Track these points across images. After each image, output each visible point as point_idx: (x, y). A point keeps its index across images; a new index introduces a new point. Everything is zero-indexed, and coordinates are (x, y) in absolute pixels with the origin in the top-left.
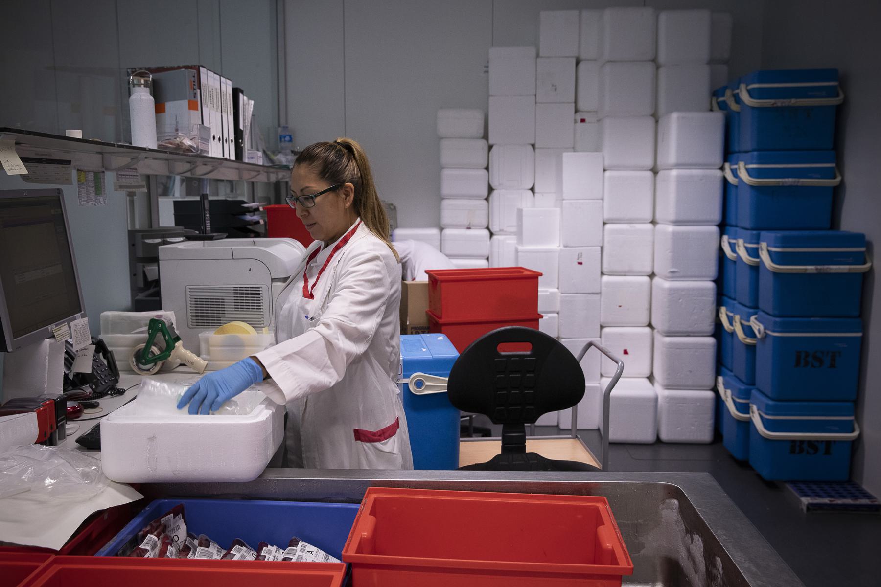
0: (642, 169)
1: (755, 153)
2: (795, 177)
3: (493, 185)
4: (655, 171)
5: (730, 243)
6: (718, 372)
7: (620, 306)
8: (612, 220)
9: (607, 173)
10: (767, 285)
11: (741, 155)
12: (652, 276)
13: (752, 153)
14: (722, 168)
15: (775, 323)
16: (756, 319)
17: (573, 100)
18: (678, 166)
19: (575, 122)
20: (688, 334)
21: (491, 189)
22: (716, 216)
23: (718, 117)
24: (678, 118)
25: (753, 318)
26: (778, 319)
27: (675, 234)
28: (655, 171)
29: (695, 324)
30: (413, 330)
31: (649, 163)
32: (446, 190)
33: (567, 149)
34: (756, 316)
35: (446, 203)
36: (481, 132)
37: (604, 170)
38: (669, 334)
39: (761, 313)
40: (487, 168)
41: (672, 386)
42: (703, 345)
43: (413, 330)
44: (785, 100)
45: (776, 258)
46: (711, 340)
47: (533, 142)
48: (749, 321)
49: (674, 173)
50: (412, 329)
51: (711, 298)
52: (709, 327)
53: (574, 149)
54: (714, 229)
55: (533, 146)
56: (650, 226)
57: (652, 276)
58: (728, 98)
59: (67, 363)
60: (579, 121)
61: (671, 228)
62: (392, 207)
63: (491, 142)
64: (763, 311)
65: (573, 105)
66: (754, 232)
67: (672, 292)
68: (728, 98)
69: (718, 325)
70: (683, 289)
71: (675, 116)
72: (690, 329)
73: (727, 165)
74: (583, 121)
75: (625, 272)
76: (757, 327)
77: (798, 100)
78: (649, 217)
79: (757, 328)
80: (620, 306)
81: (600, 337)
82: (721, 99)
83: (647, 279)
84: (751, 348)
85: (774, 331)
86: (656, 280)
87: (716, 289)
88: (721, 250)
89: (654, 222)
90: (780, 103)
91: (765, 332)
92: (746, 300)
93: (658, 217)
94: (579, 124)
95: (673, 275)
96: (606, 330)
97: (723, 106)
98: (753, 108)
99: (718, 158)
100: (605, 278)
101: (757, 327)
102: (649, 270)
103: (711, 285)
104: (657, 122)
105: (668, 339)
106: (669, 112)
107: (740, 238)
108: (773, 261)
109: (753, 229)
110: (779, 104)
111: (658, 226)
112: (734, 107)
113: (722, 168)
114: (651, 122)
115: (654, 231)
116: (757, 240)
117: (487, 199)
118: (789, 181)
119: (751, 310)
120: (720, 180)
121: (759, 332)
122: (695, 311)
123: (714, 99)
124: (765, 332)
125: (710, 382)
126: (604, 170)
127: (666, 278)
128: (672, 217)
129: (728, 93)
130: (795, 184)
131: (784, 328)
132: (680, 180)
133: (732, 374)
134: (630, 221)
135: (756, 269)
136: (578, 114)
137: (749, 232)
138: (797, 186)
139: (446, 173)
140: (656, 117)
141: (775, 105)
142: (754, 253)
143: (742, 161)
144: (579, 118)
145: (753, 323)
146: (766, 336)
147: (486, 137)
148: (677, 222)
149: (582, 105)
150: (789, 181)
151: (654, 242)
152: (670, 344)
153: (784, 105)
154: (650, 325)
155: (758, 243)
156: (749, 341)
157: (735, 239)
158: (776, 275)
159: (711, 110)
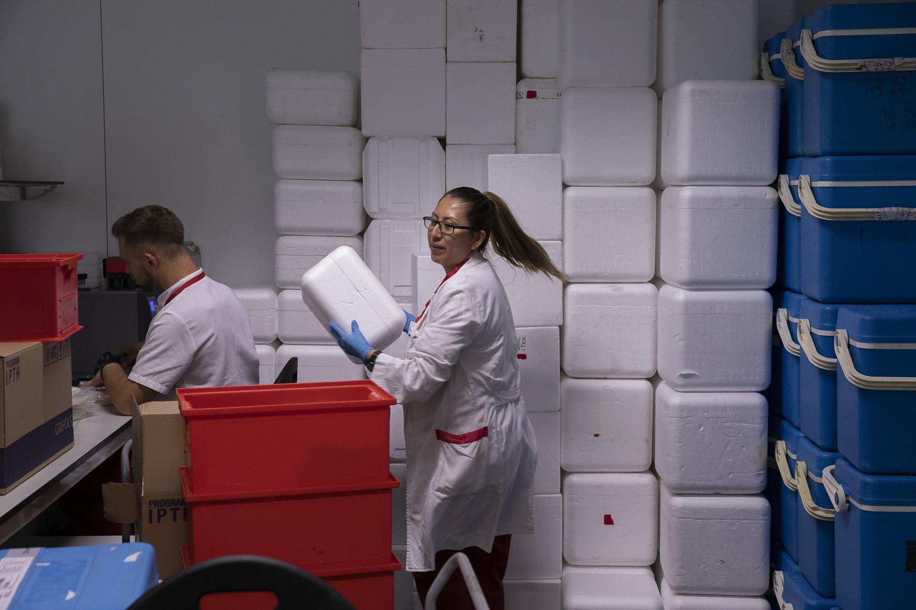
0: (633, 184)
1: (828, 159)
2: (902, 206)
3: (372, 210)
4: (657, 187)
5: (789, 322)
6: (775, 561)
7: (596, 435)
8: (580, 277)
9: (570, 192)
10: (848, 405)
11: (807, 162)
12: (654, 379)
13: (822, 159)
14: (775, 185)
15: (865, 485)
16: (832, 472)
17: (514, 57)
18: (694, 180)
19: (518, 96)
20: (717, 492)
21: (367, 220)
22: (766, 271)
23: (768, 89)
24: (693, 93)
25: (826, 471)
26: (869, 479)
27: (689, 306)
28: (657, 187)
29: (730, 473)
30: (153, 506)
31: (647, 173)
32: (284, 219)
33: (500, 147)
34: (833, 467)
35: (284, 242)
36: (348, 115)
37: (565, 186)
38: (680, 491)
39: (842, 462)
40: (360, 181)
41: (691, 589)
42: (745, 513)
43: (153, 506)
44: (882, 61)
45: (862, 361)
46: (759, 503)
47: (442, 134)
48: (820, 475)
49: (687, 192)
50: (150, 504)
51: (757, 424)
52: (755, 477)
53: (517, 147)
54: (762, 297)
55: (443, 141)
56: (649, 288)
57: (654, 379)
58: (784, 55)
59: (398, 299)
60: (525, 96)
61: (681, 295)
62: (192, 249)
63: (366, 131)
64: (845, 459)
65: (515, 65)
66: (828, 308)
67: (686, 412)
68: (784, 55)
69: (772, 472)
70: (705, 409)
71: (686, 88)
72: (719, 483)
73: (784, 179)
74: (532, 95)
75: (606, 373)
76: (834, 489)
77: (907, 60)
78: (649, 273)
79: (834, 491)
80: (596, 435)
81: (562, 491)
82: (776, 56)
83: (644, 385)
84: (826, 527)
85: (863, 502)
86: (662, 388)
87: (767, 408)
88: (774, 332)
89: (657, 280)
90: (872, 65)
91: (848, 502)
92: (816, 432)
93: (663, 273)
94: (525, 102)
95: (688, 382)
96: (574, 479)
97: (777, 69)
98: (823, 74)
99: (766, 166)
100: (570, 382)
101: (834, 489)
102: (647, 368)
103: (757, 400)
104: (660, 98)
105: (679, 501)
106: (679, 82)
107: (805, 317)
108: (857, 367)
109: (824, 302)
110: (872, 68)
111: (665, 289)
112: (794, 71)
113: (775, 185)
114: (649, 98)
115: (656, 297)
116: (832, 322)
117: (361, 235)
118: (891, 212)
119: (826, 455)
120: (770, 206)
121: (837, 502)
122: (728, 448)
123: (765, 55)
124: (848, 502)
125: (761, 583)
126: (565, 186)
127: (674, 386)
128: (684, 275)
129: (785, 45)
130: (904, 218)
131: (880, 495)
132: (696, 205)
133: (796, 568)
134: (613, 280)
135: (831, 375)
136: (522, 82)
137: (820, 307)
138: (907, 222)
139: (285, 188)
140: (657, 88)
141: (864, 70)
142: (826, 346)
143: (805, 174)
144: (524, 89)
145: (827, 482)
146: (849, 509)
147: (357, 124)
148: (693, 284)
149: (527, 68)
150: (891, 212)
151: (656, 317)
152: (684, 508)
153: (880, 69)
154: (652, 469)
155: (833, 329)
156: (822, 513)
157: (797, 316)
158: (864, 393)
159: (760, 77)
